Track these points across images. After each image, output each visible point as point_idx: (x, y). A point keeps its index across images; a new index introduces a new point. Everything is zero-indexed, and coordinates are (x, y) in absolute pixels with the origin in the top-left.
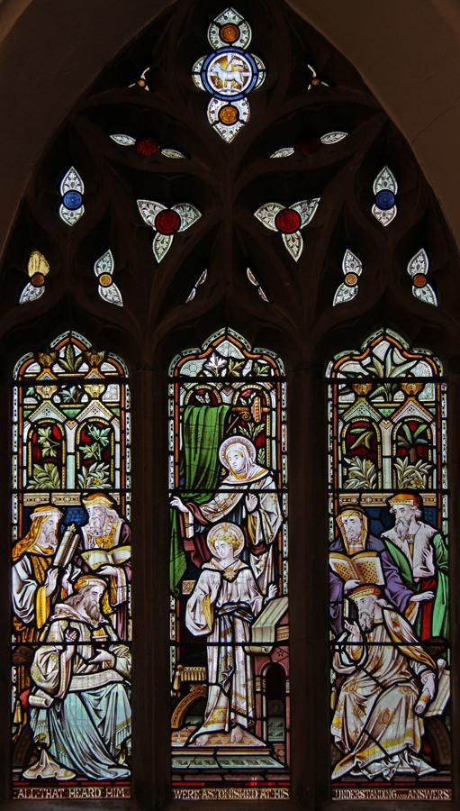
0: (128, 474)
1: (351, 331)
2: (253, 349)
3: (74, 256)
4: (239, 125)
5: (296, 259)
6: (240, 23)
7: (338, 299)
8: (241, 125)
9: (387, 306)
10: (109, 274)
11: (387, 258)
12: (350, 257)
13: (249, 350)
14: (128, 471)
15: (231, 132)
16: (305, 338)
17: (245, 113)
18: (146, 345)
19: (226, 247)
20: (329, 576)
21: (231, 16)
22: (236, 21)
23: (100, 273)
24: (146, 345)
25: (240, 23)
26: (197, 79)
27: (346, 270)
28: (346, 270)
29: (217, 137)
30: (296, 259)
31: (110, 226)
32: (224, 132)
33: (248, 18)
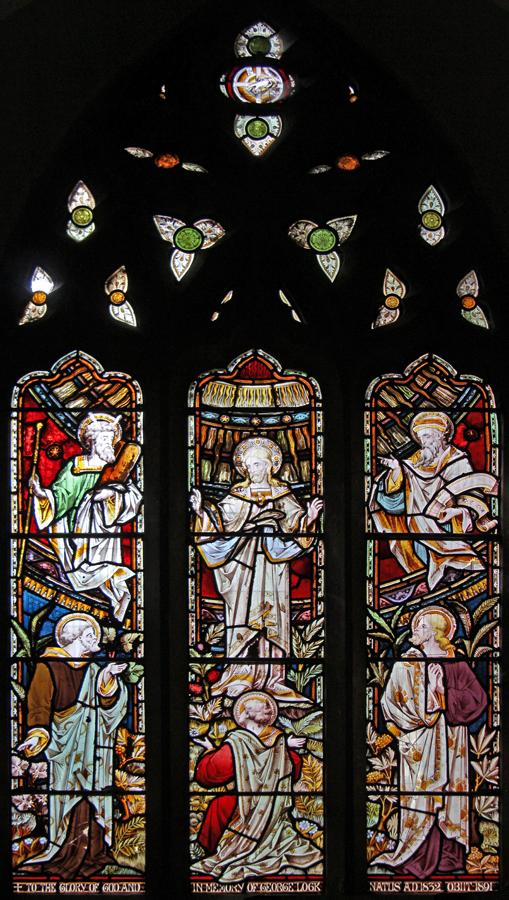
0: (367, 437)
1: (394, 349)
2: (283, 371)
3: (83, 274)
4: (269, 140)
5: (332, 281)
6: (272, 36)
7: (484, 323)
8: (272, 139)
9: (432, 324)
10: (121, 291)
11: (431, 276)
12: (390, 279)
13: (279, 370)
14: (368, 441)
15: (261, 146)
16: (345, 356)
17: (275, 127)
18: (166, 361)
19: (256, 259)
20: (11, 814)
21: (261, 30)
22: (268, 33)
23: (394, 312)
24: (166, 361)
25: (272, 36)
26: (223, 89)
27: (190, 257)
28: (190, 257)
29: (246, 151)
30: (332, 281)
31: (127, 240)
32: (253, 146)
33: (277, 30)
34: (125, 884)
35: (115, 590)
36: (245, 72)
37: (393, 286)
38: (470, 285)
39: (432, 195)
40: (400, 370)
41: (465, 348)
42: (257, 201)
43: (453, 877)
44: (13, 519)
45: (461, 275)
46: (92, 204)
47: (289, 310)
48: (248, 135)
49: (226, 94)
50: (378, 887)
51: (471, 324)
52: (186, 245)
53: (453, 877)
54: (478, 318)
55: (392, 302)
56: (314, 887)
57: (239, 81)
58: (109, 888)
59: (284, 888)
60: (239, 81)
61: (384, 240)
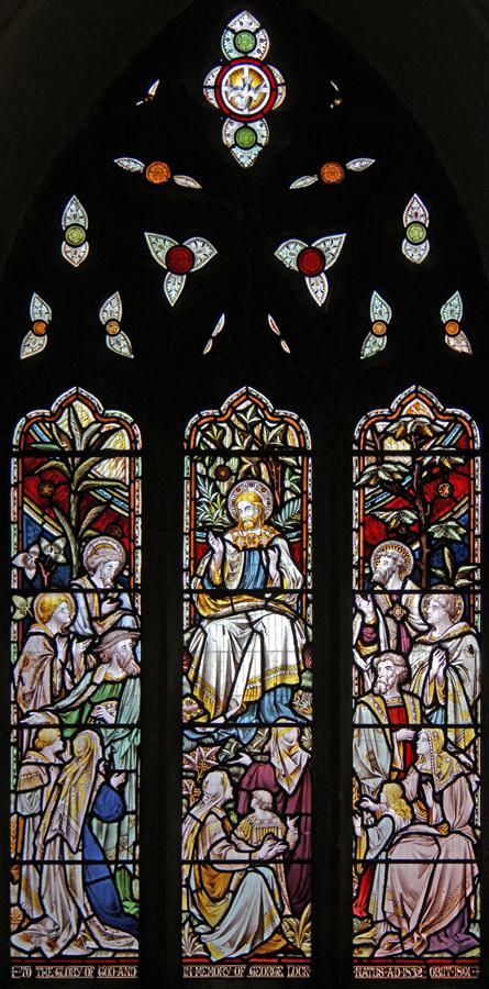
1: (381, 382)
8: (260, 149)
18: (163, 392)
19: (245, 281)
24: (163, 392)
26: (211, 94)
29: (233, 161)
31: (118, 260)
34: (121, 968)
35: (22, 658)
36: (242, 69)
37: (380, 310)
38: (452, 309)
39: (415, 204)
40: (388, 406)
41: (448, 380)
42: (246, 209)
43: (276, 961)
44: (354, 502)
45: (443, 299)
46: (84, 222)
47: (278, 339)
48: (236, 144)
49: (272, 68)
50: (361, 973)
51: (456, 352)
52: (179, 260)
53: (276, 961)
54: (459, 344)
55: (379, 328)
56: (299, 972)
57: (251, 70)
58: (104, 973)
59: (71, 973)
60: (251, 70)
61: (373, 262)
